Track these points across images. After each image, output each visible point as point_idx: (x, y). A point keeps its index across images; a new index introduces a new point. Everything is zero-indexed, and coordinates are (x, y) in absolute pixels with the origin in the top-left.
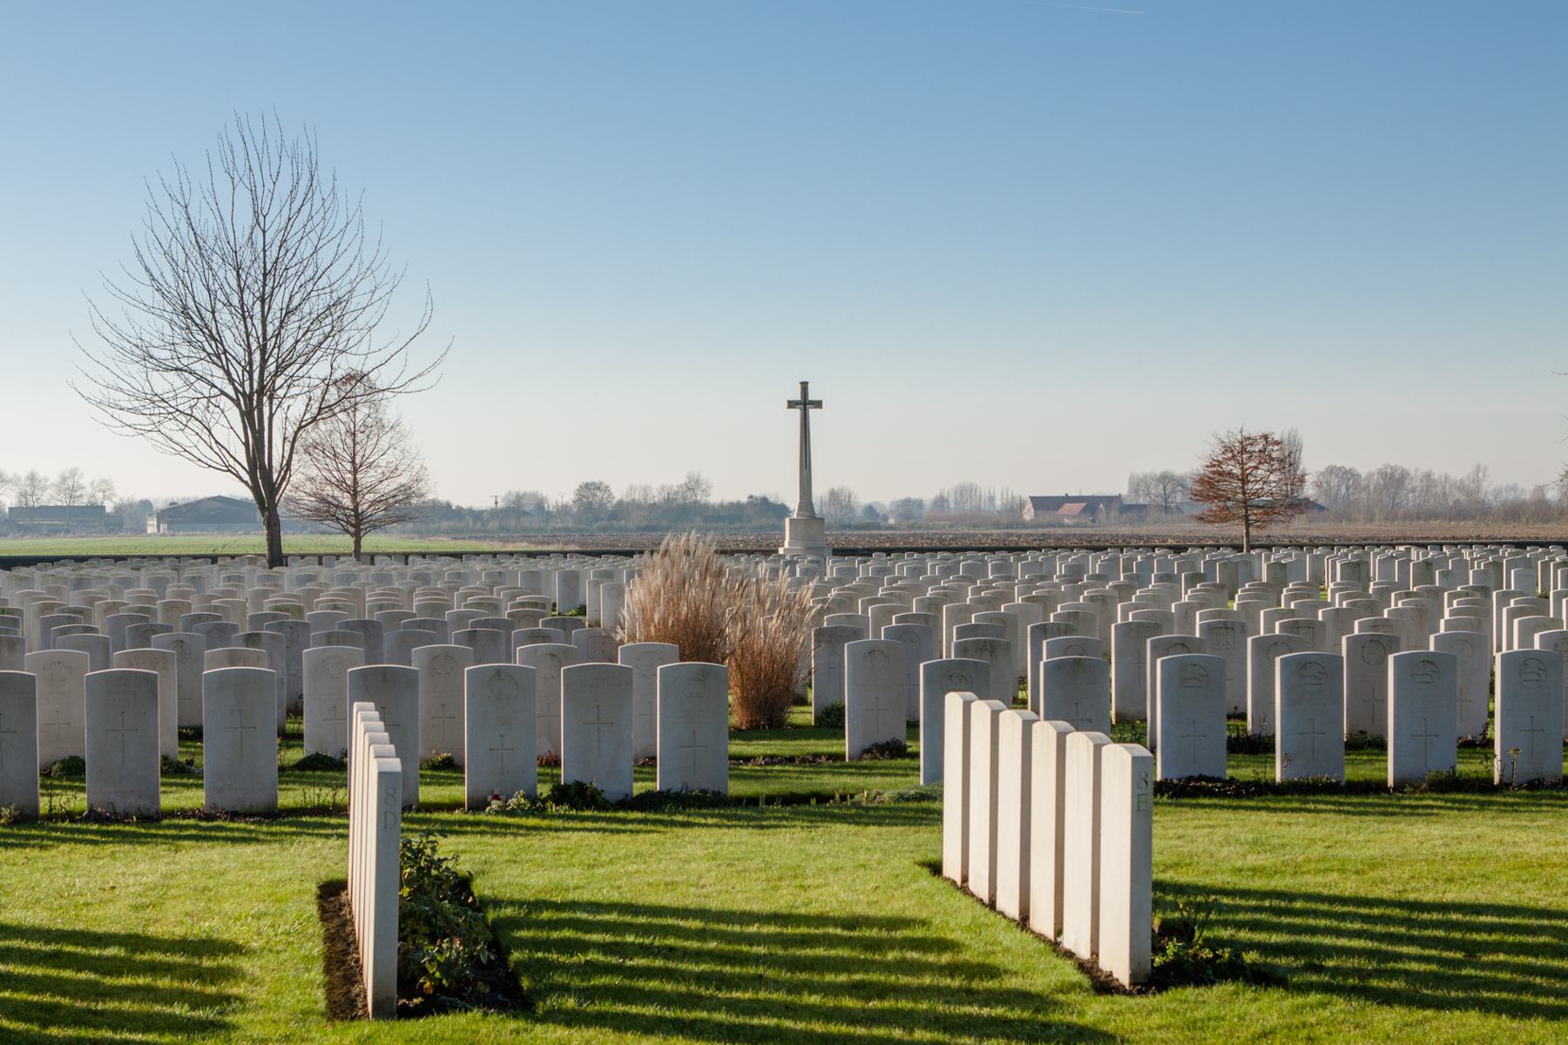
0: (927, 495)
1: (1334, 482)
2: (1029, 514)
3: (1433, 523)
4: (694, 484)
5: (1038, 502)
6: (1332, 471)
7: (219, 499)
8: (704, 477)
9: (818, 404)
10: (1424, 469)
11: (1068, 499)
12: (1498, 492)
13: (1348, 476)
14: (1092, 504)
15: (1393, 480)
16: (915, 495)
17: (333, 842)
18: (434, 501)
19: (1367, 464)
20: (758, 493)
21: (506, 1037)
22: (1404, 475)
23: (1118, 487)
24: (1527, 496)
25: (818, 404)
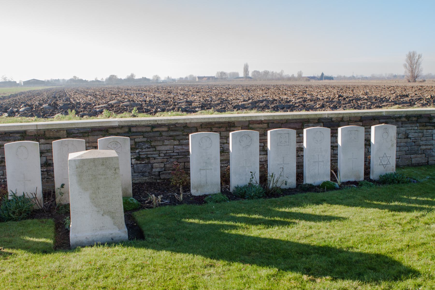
0: (184, 77)
1: (255, 73)
2: (197, 80)
3: (273, 81)
4: (132, 75)
5: (199, 78)
6: (255, 71)
7: (34, 79)
8: (134, 74)
9: (323, 74)
10: (272, 71)
11: (205, 77)
12: (285, 76)
13: (258, 72)
14: (209, 78)
15: (266, 73)
16: (181, 77)
17: (137, 182)
18: (106, 79)
19: (261, 70)
20: (144, 76)
21: (234, 284)
22: (268, 72)
23: (214, 74)
24: (290, 76)
25: (323, 74)
